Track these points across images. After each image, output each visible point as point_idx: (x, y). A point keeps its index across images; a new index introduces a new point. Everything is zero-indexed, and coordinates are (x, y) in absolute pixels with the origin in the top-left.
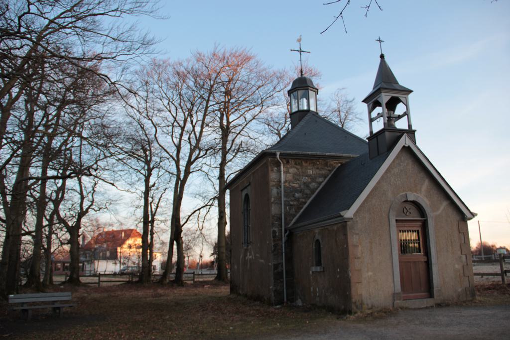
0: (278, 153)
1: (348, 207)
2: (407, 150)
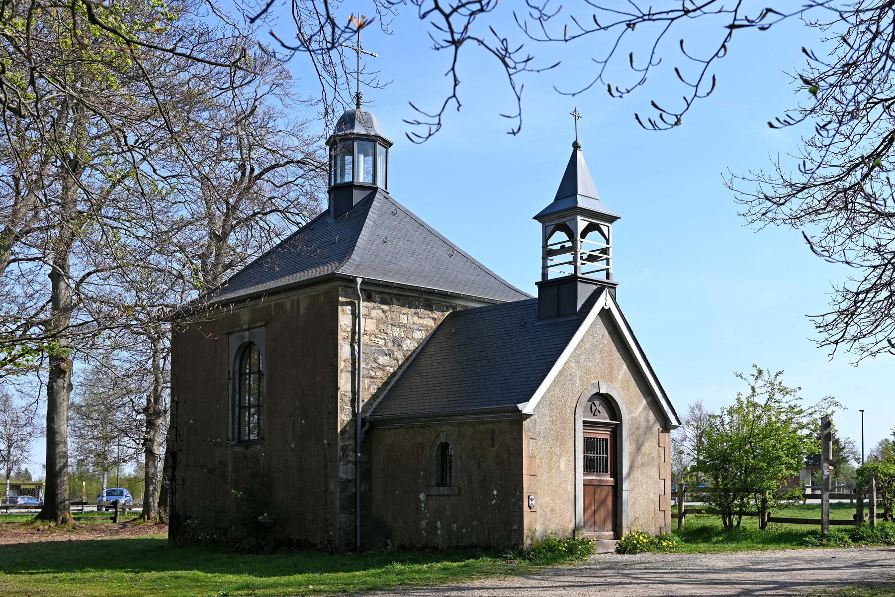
0: (359, 281)
1: (527, 399)
2: (606, 314)
